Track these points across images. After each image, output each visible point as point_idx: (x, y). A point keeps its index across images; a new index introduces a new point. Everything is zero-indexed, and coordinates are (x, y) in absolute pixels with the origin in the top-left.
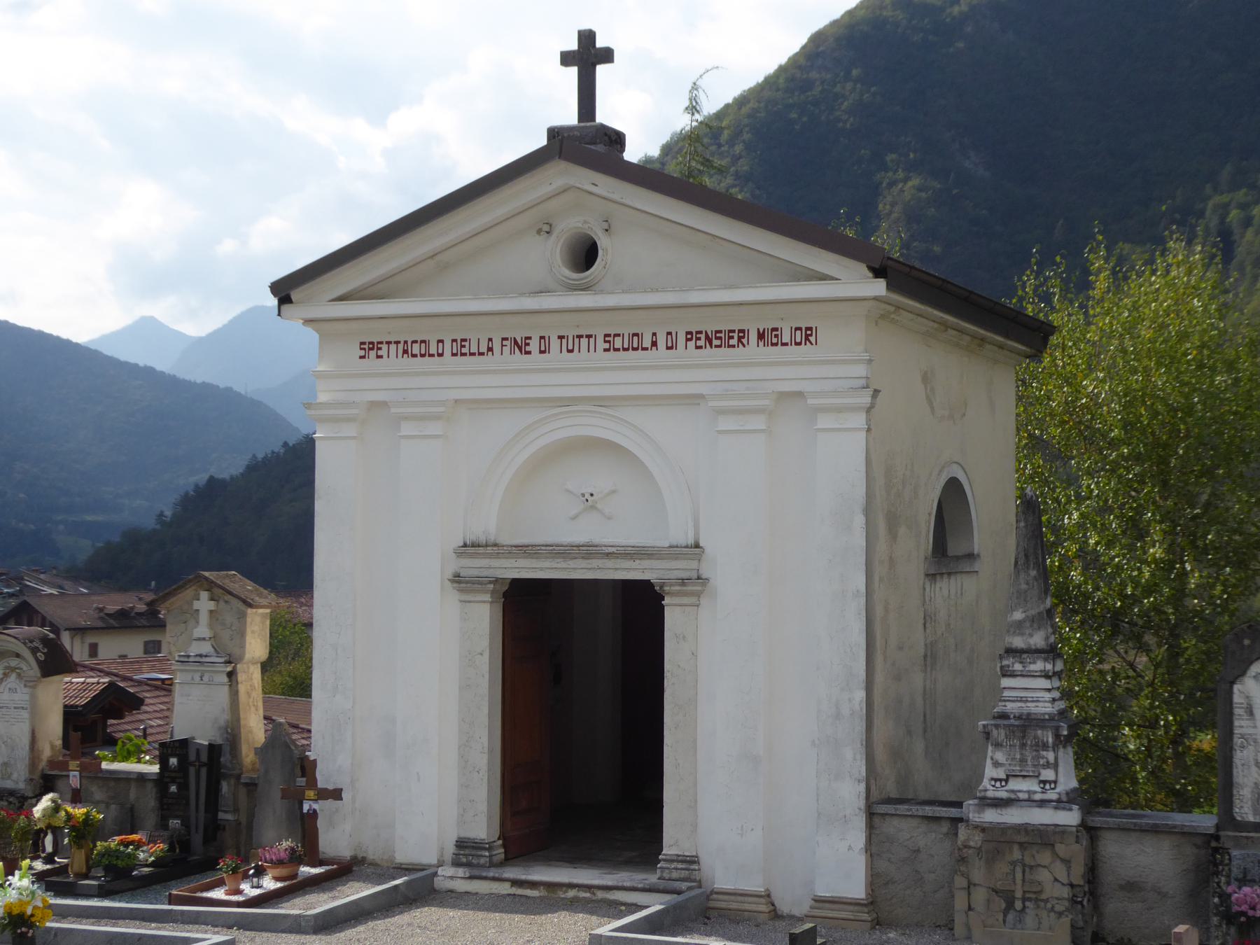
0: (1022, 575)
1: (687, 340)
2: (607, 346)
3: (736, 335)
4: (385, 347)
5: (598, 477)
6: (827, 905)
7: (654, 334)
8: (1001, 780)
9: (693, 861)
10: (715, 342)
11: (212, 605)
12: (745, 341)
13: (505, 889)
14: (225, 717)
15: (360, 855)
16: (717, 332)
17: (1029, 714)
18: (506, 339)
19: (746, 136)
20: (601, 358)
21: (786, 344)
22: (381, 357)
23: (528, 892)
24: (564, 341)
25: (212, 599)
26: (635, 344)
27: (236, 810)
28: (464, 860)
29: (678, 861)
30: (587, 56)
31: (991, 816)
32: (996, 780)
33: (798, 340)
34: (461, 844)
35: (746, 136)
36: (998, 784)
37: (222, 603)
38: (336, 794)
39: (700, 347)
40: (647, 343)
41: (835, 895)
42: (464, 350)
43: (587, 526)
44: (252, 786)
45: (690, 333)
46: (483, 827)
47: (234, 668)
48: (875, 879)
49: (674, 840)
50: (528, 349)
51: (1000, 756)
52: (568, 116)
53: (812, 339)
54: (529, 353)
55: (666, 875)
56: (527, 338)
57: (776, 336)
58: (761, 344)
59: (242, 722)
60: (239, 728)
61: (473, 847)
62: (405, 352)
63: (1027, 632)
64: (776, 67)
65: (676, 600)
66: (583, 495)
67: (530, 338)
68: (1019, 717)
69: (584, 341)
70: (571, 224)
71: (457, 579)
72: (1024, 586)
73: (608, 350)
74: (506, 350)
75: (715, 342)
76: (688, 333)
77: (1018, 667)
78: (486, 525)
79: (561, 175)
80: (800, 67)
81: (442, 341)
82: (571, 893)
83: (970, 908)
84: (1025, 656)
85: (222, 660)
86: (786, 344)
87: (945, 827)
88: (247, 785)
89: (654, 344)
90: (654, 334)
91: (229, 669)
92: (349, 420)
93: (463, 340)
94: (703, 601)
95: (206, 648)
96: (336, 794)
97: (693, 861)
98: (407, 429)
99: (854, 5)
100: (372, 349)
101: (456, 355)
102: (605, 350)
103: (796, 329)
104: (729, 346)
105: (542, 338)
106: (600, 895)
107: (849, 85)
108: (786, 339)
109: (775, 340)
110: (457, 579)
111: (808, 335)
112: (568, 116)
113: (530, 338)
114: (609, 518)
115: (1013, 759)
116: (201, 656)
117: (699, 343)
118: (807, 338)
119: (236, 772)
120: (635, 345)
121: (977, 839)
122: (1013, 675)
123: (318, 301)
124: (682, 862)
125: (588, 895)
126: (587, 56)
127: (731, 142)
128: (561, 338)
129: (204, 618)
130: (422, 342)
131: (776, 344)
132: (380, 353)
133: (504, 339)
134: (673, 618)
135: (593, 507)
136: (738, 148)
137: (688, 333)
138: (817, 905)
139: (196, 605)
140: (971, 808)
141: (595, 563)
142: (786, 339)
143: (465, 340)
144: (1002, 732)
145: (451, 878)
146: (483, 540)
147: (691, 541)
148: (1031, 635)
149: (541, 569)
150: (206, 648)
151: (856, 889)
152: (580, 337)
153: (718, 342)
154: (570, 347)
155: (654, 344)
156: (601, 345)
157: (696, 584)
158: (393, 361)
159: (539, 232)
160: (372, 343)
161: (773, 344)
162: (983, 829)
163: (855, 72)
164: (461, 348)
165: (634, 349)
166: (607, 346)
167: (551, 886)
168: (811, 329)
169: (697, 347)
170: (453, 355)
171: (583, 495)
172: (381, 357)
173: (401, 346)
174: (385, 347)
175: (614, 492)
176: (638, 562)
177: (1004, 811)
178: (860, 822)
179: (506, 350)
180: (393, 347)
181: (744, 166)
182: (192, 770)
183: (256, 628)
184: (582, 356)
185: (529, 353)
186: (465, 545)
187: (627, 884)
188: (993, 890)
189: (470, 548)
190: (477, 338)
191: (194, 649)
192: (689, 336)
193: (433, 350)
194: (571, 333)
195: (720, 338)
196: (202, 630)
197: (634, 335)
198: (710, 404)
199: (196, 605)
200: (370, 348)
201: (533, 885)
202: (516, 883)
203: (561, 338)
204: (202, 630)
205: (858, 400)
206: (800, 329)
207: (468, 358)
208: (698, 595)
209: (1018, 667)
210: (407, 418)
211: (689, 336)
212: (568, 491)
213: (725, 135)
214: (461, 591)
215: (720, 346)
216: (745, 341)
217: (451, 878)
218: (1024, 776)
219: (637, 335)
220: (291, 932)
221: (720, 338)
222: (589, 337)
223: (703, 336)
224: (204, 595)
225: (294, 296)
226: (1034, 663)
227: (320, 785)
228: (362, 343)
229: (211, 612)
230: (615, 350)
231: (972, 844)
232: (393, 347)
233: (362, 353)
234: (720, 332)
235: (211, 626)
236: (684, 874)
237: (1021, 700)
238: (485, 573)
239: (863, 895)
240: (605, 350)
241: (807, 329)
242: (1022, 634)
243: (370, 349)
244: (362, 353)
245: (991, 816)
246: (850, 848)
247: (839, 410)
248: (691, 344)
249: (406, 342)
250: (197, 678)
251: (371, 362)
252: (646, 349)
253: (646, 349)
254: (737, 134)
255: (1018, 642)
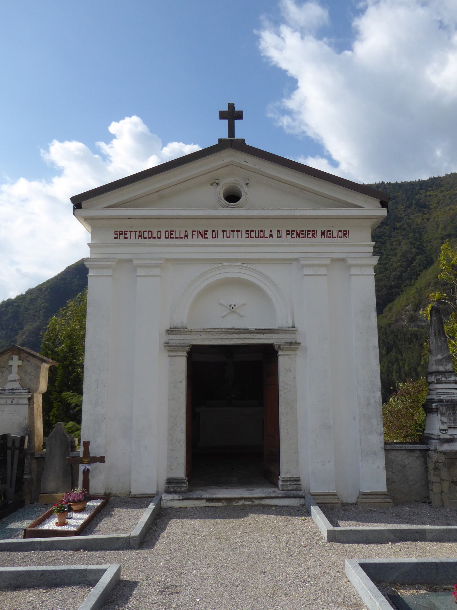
0: (439, 340)
1: (287, 234)
2: (247, 236)
3: (311, 233)
4: (129, 234)
5: (237, 297)
6: (369, 496)
7: (271, 231)
8: (445, 430)
9: (297, 480)
10: (301, 236)
11: (20, 363)
12: (315, 235)
13: (203, 503)
14: (25, 422)
15: (108, 492)
16: (301, 231)
17: (452, 400)
18: (195, 231)
19: (49, 290)
20: (244, 240)
21: (335, 237)
22: (127, 238)
23: (216, 504)
24: (225, 233)
25: (19, 360)
26: (261, 235)
27: (30, 473)
28: (172, 490)
29: (290, 481)
30: (232, 115)
31: (446, 447)
32: (443, 430)
33: (340, 236)
34: (170, 481)
35: (49, 290)
36: (444, 432)
37: (26, 362)
38: (102, 460)
39: (294, 238)
40: (267, 234)
41: (372, 491)
42: (172, 236)
43: (236, 319)
44: (41, 459)
45: (289, 231)
46: (180, 472)
47: (32, 396)
48: (389, 482)
49: (286, 470)
50: (206, 236)
51: (444, 419)
52: (225, 136)
53: (347, 235)
54: (207, 238)
55: (285, 488)
56: (205, 231)
57: (330, 234)
58: (323, 237)
59: (35, 424)
60: (34, 427)
61: (178, 483)
62: (140, 236)
63: (444, 364)
64: (37, 285)
65: (285, 353)
66: (230, 306)
67: (207, 231)
68: (448, 401)
69: (235, 233)
70: (227, 181)
71: (167, 345)
72: (440, 344)
73: (248, 237)
74: (195, 236)
75: (301, 236)
76: (287, 231)
77: (444, 379)
78: (182, 319)
79: (228, 157)
80: (64, 275)
81: (160, 231)
82: (241, 503)
83: (442, 492)
84: (446, 374)
85: (26, 391)
86: (335, 237)
87: (417, 454)
88: (37, 458)
89: (271, 235)
90: (271, 231)
91: (30, 396)
92: (107, 267)
93: (171, 231)
94: (298, 353)
95: (16, 385)
96: (102, 460)
97: (297, 480)
98: (141, 272)
99: (34, 287)
100: (122, 234)
101: (168, 238)
102: (246, 237)
103: (339, 231)
104: (308, 237)
105: (213, 231)
106: (257, 502)
107: (76, 280)
108: (335, 235)
109: (329, 236)
110: (167, 345)
111: (345, 234)
112: (225, 136)
113: (207, 231)
114: (242, 317)
115: (450, 420)
116: (13, 389)
117: (293, 236)
118: (344, 235)
119: (32, 451)
120: (262, 236)
121: (442, 458)
122: (442, 383)
123: (96, 209)
124: (293, 481)
125: (250, 503)
126: (232, 115)
127: (45, 291)
128: (223, 231)
129: (15, 369)
130: (149, 231)
131: (330, 237)
132: (126, 236)
133: (193, 231)
134: (283, 361)
135: (234, 312)
136: (46, 293)
137: (287, 231)
138: (362, 496)
139: (10, 363)
140: (437, 444)
141: (242, 336)
142: (335, 235)
143: (173, 231)
144: (444, 408)
145: (171, 500)
146: (180, 326)
147: (290, 325)
148: (446, 365)
149: (214, 339)
150: (16, 385)
151: (382, 487)
152: (233, 231)
153: (302, 236)
154: (228, 236)
155: (271, 235)
156: (244, 235)
157: (293, 346)
158: (133, 240)
159: (212, 184)
160: (122, 232)
161: (329, 237)
162: (444, 453)
163: (77, 277)
164: (170, 235)
165: (261, 237)
166: (247, 236)
167: (229, 500)
168: (346, 231)
169: (292, 238)
170: (166, 238)
171: (230, 306)
172: (127, 238)
173: (137, 234)
174: (129, 234)
175: (244, 305)
176: (265, 335)
177: (452, 444)
178: (382, 454)
179: (195, 236)
180: (133, 234)
181: (47, 298)
182: (9, 452)
183: (43, 375)
184: (234, 240)
185: (207, 238)
186: (170, 329)
187: (273, 495)
188: (452, 482)
189: (173, 330)
190: (179, 229)
191: (9, 386)
192: (288, 232)
193: (155, 235)
194: (228, 229)
195: (303, 234)
196: (14, 375)
197: (261, 231)
198: (302, 262)
199: (10, 363)
200: (120, 234)
201: (219, 500)
202: (208, 500)
203: (223, 231)
204: (14, 375)
205: (372, 262)
206: (341, 231)
207: (174, 239)
208: (296, 349)
209: (444, 379)
210: (140, 266)
211: (288, 232)
212: (221, 304)
213: (44, 289)
214: (169, 351)
215: (303, 237)
216: (315, 235)
217: (171, 501)
218: (454, 428)
219: (262, 231)
220: (122, 549)
221: (303, 234)
222: (238, 231)
223: (295, 233)
224: (16, 357)
225: (83, 205)
226: (451, 377)
227: (91, 455)
228: (115, 232)
229: (19, 366)
230: (251, 237)
231: (440, 461)
232: (133, 234)
233: (116, 236)
234: (303, 231)
235: (18, 373)
236: (295, 487)
237: (446, 394)
238: (183, 342)
239: (386, 490)
240: (246, 237)
241: (344, 231)
242: (442, 365)
243: (120, 234)
244: (116, 236)
245: (446, 447)
246: (378, 467)
247: (361, 266)
248: (289, 236)
249: (140, 231)
250: (9, 401)
251: (121, 240)
252: (267, 237)
253: (267, 237)
254: (47, 289)
255: (441, 368)
